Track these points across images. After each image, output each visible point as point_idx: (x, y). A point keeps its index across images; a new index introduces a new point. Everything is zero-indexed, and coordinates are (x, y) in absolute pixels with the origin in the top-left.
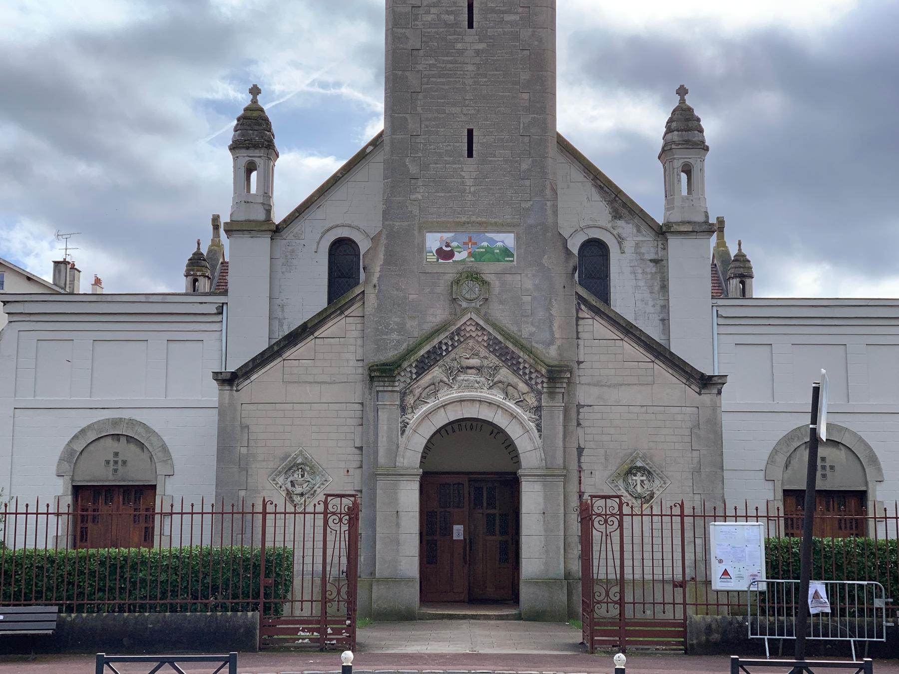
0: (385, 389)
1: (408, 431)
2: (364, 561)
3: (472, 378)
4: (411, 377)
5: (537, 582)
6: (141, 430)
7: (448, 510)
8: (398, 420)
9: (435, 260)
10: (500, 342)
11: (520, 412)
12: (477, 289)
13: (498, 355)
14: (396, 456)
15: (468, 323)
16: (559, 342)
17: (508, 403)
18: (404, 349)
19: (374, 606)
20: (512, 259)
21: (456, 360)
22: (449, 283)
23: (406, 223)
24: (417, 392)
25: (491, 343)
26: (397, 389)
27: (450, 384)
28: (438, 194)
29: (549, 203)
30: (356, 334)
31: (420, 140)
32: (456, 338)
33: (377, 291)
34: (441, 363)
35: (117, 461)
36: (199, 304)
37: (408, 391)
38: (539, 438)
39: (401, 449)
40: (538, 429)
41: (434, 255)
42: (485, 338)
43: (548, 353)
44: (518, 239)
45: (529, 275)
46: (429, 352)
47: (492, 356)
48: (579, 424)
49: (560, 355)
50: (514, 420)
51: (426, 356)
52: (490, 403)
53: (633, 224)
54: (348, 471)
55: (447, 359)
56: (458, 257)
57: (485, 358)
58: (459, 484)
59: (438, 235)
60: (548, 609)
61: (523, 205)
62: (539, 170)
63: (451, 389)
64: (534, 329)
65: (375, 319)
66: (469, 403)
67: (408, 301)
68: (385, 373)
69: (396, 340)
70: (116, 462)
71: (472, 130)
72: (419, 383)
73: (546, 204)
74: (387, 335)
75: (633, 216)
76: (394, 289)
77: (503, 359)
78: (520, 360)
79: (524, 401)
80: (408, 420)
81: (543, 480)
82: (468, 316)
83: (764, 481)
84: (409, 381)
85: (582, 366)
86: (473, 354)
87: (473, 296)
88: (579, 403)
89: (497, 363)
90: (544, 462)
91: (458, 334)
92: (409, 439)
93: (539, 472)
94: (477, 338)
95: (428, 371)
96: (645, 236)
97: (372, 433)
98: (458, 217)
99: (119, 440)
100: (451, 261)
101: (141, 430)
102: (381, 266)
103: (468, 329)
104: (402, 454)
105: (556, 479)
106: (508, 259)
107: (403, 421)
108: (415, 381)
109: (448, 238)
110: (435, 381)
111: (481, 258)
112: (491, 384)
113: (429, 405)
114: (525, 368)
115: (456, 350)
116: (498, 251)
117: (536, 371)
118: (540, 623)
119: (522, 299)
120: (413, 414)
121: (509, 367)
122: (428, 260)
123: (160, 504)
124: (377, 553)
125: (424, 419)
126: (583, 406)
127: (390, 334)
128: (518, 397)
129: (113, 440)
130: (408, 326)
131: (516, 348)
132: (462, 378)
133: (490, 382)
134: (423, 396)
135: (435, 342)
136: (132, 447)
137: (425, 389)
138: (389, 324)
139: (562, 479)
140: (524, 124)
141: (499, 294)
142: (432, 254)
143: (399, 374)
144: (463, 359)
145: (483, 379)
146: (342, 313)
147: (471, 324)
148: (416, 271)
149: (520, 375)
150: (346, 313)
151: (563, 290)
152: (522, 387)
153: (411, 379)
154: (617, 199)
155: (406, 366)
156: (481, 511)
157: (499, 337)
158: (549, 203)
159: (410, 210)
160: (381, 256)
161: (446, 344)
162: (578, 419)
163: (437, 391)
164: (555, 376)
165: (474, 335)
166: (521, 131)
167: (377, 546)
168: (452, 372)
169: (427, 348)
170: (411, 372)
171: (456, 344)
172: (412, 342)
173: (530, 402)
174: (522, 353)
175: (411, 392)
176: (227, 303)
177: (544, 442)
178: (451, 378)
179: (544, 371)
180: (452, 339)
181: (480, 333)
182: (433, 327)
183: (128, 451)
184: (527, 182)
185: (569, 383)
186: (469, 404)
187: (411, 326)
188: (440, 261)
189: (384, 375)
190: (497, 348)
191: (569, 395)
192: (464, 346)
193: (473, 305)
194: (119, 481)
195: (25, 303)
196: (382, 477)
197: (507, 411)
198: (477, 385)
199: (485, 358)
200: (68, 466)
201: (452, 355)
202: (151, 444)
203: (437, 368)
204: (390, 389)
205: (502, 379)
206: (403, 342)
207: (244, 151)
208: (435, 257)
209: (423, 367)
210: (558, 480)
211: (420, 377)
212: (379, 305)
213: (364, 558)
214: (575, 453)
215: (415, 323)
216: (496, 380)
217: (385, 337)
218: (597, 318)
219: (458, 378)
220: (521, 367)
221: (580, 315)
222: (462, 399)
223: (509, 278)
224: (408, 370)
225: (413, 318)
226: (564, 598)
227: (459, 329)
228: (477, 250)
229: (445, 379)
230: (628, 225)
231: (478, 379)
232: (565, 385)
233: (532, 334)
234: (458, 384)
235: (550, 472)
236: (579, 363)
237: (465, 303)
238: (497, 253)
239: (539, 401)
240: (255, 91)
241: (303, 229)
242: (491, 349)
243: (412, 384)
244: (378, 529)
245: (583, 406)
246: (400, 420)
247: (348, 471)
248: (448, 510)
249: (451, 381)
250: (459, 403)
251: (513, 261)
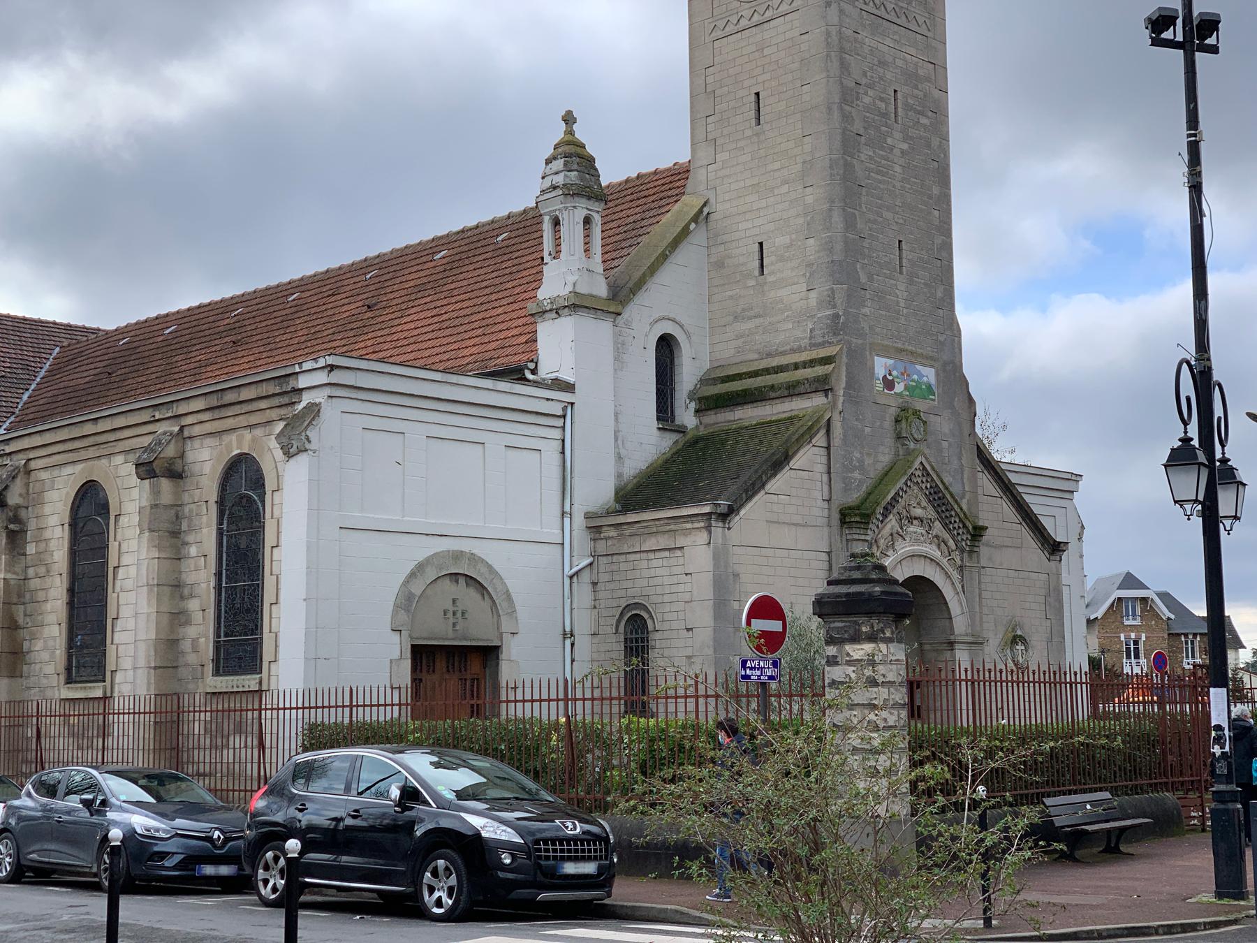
6: (484, 570)
35: (456, 613)
36: (545, 401)
44: (937, 375)
47: (930, 508)
70: (454, 613)
78: (953, 513)
83: (390, 630)
99: (457, 582)
100: (892, 392)
101: (484, 570)
119: (941, 444)
123: (507, 673)
129: (451, 581)
136: (473, 593)
149: (950, 529)
152: (951, 543)
176: (572, 404)
179: (970, 528)
183: (469, 597)
188: (886, 391)
194: (460, 640)
195: (358, 372)
200: (406, 617)
202: (495, 589)
207: (584, 200)
240: (569, 119)
251: (934, 400)
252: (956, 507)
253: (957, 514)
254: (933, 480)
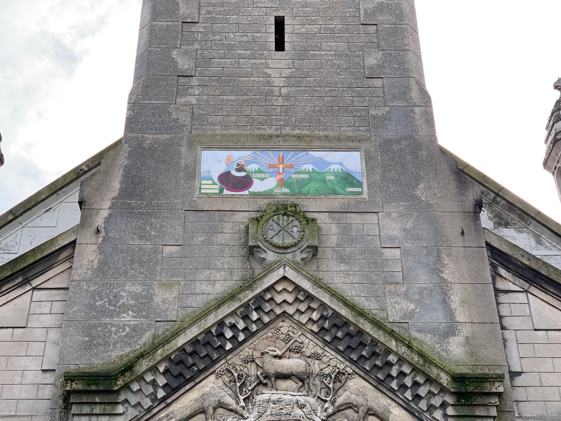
3: (287, 397)
4: (154, 394)
9: (217, 191)
10: (347, 323)
12: (295, 229)
13: (341, 348)
15: (279, 288)
16: (466, 330)
18: (145, 345)
20: (360, 190)
21: (253, 361)
22: (242, 227)
23: (167, 136)
25: (326, 325)
27: (239, 409)
28: (225, 98)
29: (417, 110)
31: (199, 28)
32: (255, 316)
33: (100, 240)
34: (220, 366)
41: (214, 184)
42: (315, 316)
44: (368, 159)
45: (393, 215)
46: (194, 342)
47: (330, 353)
49: (472, 354)
51: (189, 349)
53: (528, 233)
55: (235, 359)
56: (258, 186)
57: (316, 357)
59: (224, 154)
61: (373, 112)
62: (396, 66)
64: (412, 306)
65: (91, 289)
67: (160, 257)
68: (97, 384)
71: (283, 18)
72: (170, 409)
73: (413, 111)
75: (526, 222)
76: (135, 236)
77: (354, 357)
78: (392, 358)
82: (280, 273)
84: (147, 403)
85: (518, 381)
87: (289, 241)
89: (342, 367)
91: (258, 309)
94: (296, 317)
95: (192, 384)
96: (550, 249)
98: (259, 129)
100: (246, 192)
102: (113, 199)
103: (279, 299)
106: (351, 190)
108: (163, 405)
109: (240, 158)
111: (302, 187)
112: (330, 411)
114: (402, 374)
115: (254, 341)
116: (332, 178)
117: (429, 380)
121: (367, 375)
122: (202, 191)
130: (157, 300)
132: (265, 397)
133: (326, 405)
140: (365, 10)
141: (338, 245)
142: (211, 182)
144: (267, 358)
146: (27, 281)
147: (285, 289)
148: (180, 206)
149: (392, 390)
150: (35, 283)
151: (460, 237)
154: (499, 199)
155: (144, 368)
157: (344, 312)
158: (417, 110)
159: (175, 117)
160: (116, 185)
161: (233, 327)
164: (470, 389)
165: (291, 310)
166: (362, 19)
168: (243, 385)
169: (193, 332)
170: (154, 383)
174: (394, 343)
179: (445, 379)
180: (246, 317)
181: (303, 307)
184: (378, 83)
187: (164, 301)
188: (226, 192)
189: (93, 388)
190: (340, 334)
192: (270, 334)
199: (316, 357)
201: (246, 351)
205: (354, 398)
206: (145, 331)
208: (217, 187)
209: (181, 374)
211: (173, 397)
215: (171, 295)
217: (108, 320)
219: (258, 398)
220: (394, 373)
221: (501, 285)
223: (355, 219)
224: (149, 378)
225: (168, 286)
227: (259, 298)
228: (294, 176)
229: (229, 400)
230: (521, 235)
231: (302, 400)
233: (411, 314)
234: (256, 409)
236: (514, 375)
237: (272, 253)
238: (330, 181)
241: (18, 240)
242: (328, 338)
243: (155, 411)
249: (243, 404)
251: (361, 193)
252: (393, 345)
253: (401, 360)
254: (323, 306)
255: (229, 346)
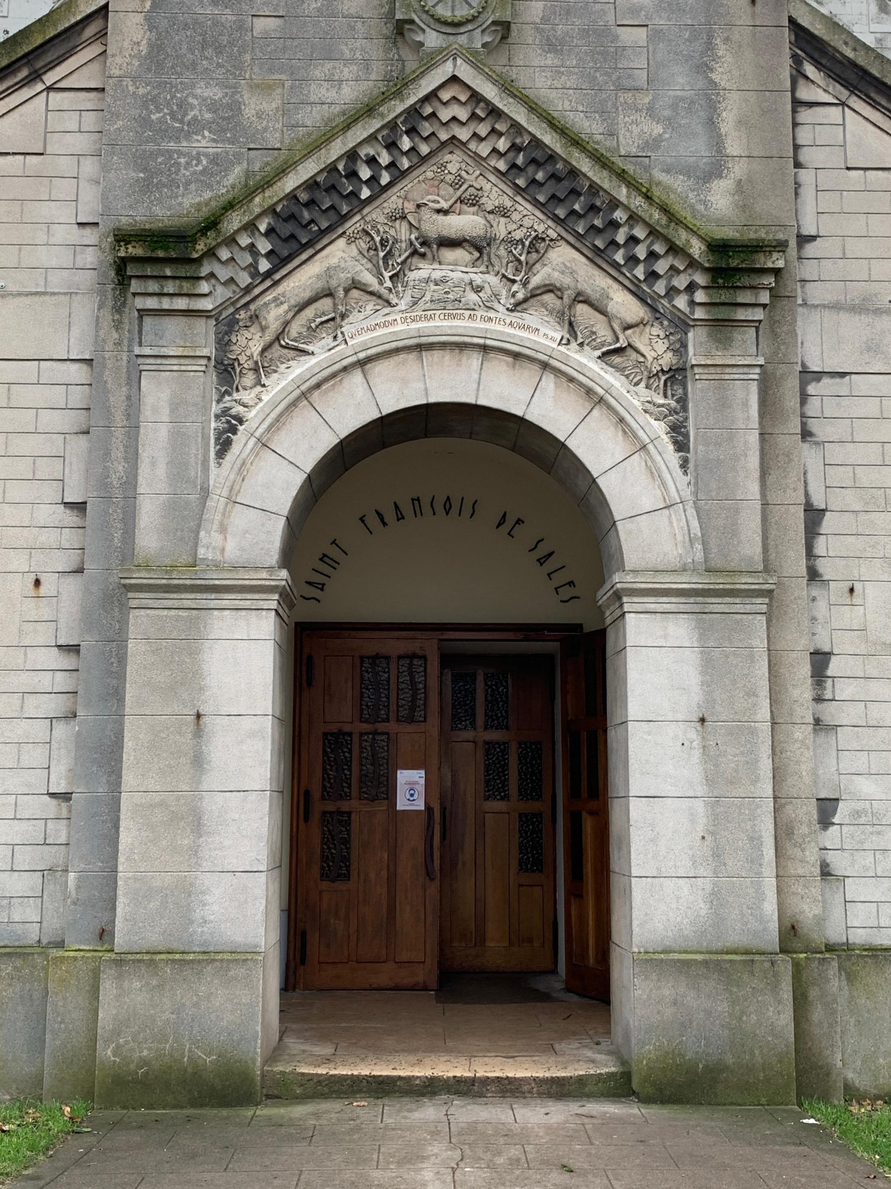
0: (166, 304)
1: (241, 443)
2: (78, 887)
3: (457, 275)
5: (687, 963)
7: (381, 727)
8: (206, 409)
10: (552, 157)
11: (617, 384)
13: (542, 198)
14: (199, 526)
15: (445, 96)
16: (738, 170)
17: (577, 356)
19: (106, 1053)
21: (404, 217)
24: (274, 316)
25: (520, 160)
26: (206, 304)
30: (81, 143)
32: (406, 143)
34: (354, 225)
37: (243, 315)
38: (678, 472)
39: (217, 502)
40: (675, 442)
42: (502, 144)
43: (705, 203)
46: (311, 185)
47: (524, 207)
48: (806, 434)
50: (596, 412)
51: (304, 197)
52: (516, 356)
54: (37, 583)
55: (376, 214)
57: (503, 212)
58: (414, 656)
60: (730, 1060)
63: (387, 310)
64: (658, 129)
65: (141, 91)
66: (447, 357)
67: (248, 38)
68: (166, 249)
69: (206, 155)
72: (280, 289)
74: (178, 139)
77: (561, 212)
78: (619, 215)
79: (630, 351)
80: (241, 409)
81: (696, 608)
84: (244, 279)
85: (810, 249)
86: (461, 200)
88: (803, 365)
89: (541, 228)
90: (699, 547)
91: (412, 131)
92: (242, 469)
93: (683, 582)
94: (473, 146)
95: (310, 252)
97: (118, 453)
103: (445, 115)
104: (218, 517)
105: (738, 605)
107: (225, 412)
108: (268, 283)
110: (334, 283)
112: (520, 296)
113: (312, 361)
115: (406, 185)
117: (673, 249)
118: (705, 1111)
119: (616, 38)
120: (259, 389)
121: (579, 242)
124: (121, 859)
125: (294, 404)
126: (819, 376)
127: (188, 136)
128: (610, 338)
131: (605, 173)
132: (423, 274)
133: (515, 288)
134: (295, 328)
135: (337, 149)
137: (302, 307)
138: (183, 105)
139: (761, 606)
141: (545, 20)
143: (211, 253)
144: (426, 214)
145: (493, 279)
146: (36, 76)
149: (616, 265)
150: (50, 78)
153: (253, 269)
155: (236, 225)
156: (469, 734)
157: (549, 138)
161: (372, 161)
162: (803, 416)
163: (343, 316)
165: (463, 134)
167: (125, 839)
170: (252, 248)
171: (405, 163)
172: (258, 162)
173: (650, 355)
174: (624, 190)
175: (255, 318)
177: (696, 485)
178: (387, 275)
179: (697, 248)
180: (392, 146)
182: (331, 120)
185: (775, 295)
186: (447, 358)
189: (161, 254)
190: (540, 176)
191: (775, 335)
192: (430, 174)
193: (463, 39)
196: (144, 598)
197: (571, 380)
198: (472, 297)
199: (503, 212)
201: (393, 201)
203: (342, 242)
204: (181, 303)
205: (557, 278)
209: (293, 236)
210: (748, 608)
211: (284, 272)
212: (157, 49)
213: (79, 879)
214: (798, 516)
215: (271, 104)
216: (535, 281)
218: (856, 103)
219: (413, 276)
221: (805, 93)
222: (424, 340)
225: (265, 88)
226: (785, 1019)
227: (413, 112)
231: (478, 279)
232: (765, 297)
233: (655, 143)
234: (409, 292)
235: (720, 582)
239: (680, 349)
242: (521, 182)
243: (257, 291)
244: (129, 779)
245: (819, 376)
246: (215, 409)
247: (37, 583)
248: (381, 727)
249: (388, 284)
250: (412, 356)
252: (622, 193)
253: (634, 218)
255: (365, 193)
